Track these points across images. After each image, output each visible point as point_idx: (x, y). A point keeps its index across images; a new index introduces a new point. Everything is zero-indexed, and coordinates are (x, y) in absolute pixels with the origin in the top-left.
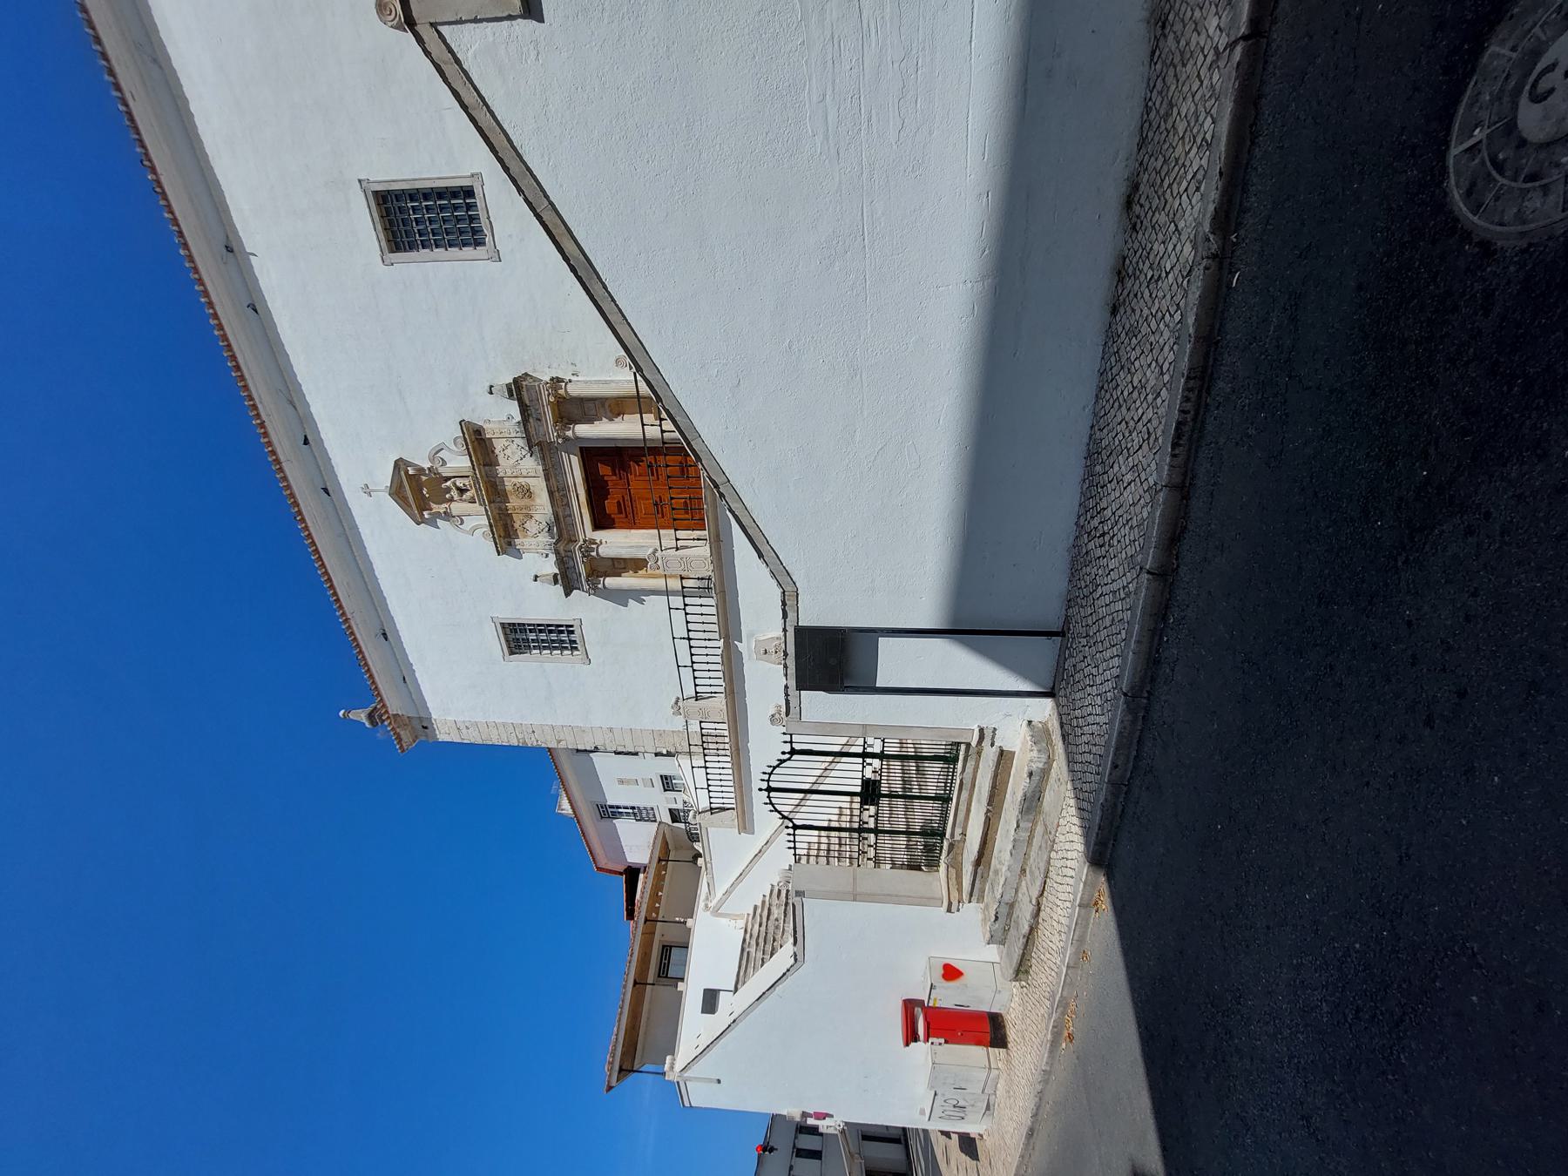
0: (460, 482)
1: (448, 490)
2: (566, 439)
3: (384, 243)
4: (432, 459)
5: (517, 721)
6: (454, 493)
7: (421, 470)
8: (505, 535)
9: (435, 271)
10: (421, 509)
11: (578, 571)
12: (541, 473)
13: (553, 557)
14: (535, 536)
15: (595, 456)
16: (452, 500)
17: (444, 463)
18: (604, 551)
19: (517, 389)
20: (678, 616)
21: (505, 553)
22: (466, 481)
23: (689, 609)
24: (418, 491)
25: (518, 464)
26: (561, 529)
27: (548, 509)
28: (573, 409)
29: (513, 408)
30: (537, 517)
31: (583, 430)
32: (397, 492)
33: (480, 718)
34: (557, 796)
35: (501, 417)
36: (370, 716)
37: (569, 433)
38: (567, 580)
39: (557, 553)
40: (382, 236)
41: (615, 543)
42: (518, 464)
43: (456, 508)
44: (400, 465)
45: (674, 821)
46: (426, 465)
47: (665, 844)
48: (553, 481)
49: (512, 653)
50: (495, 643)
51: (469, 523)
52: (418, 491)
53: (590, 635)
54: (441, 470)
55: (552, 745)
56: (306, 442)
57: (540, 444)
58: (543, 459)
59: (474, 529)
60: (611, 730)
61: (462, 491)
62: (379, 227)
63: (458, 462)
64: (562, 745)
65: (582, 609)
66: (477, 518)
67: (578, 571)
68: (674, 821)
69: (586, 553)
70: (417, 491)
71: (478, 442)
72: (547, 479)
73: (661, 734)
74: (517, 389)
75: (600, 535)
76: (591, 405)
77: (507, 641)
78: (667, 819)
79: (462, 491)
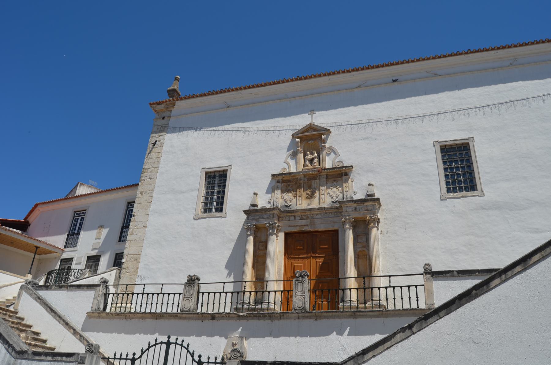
0: (316, 160)
1: (312, 154)
2: (344, 223)
3: (444, 144)
4: (330, 148)
5: (160, 170)
6: (310, 157)
7: (324, 142)
8: (284, 182)
9: (433, 168)
10: (301, 138)
11: (258, 223)
12: (322, 206)
13: (268, 206)
14: (283, 198)
15: (333, 239)
16: (305, 155)
17: (328, 154)
18: (272, 239)
19: (371, 201)
20: (219, 288)
21: (272, 179)
22: (317, 164)
23: (223, 295)
24: (311, 140)
25: (326, 197)
26: (286, 213)
27: (299, 207)
28: (363, 228)
29: (360, 196)
30: (294, 200)
31: (350, 235)
32: (311, 127)
33: (165, 148)
34: (91, 186)
35: (356, 189)
36: (174, 90)
37: (348, 226)
38: (252, 212)
39: (269, 210)
40: (447, 143)
41: (276, 245)
42: (326, 197)
43: (301, 156)
44: (327, 131)
45: (62, 260)
46: (327, 145)
47: (45, 252)
48: (318, 212)
49: (206, 173)
50: (215, 164)
51: (292, 163)
52: (311, 140)
53: (214, 222)
54: (324, 153)
55: (140, 189)
56: (394, 81)
57: (341, 207)
58: (331, 208)
59: (288, 164)
60: (145, 227)
61: (311, 161)
62: (452, 143)
63: (328, 162)
64: (139, 195)
65: (233, 220)
66: (295, 166)
67: (258, 223)
68: (62, 260)
69: (272, 226)
70: (311, 138)
71: (340, 175)
72: (319, 209)
73: (137, 260)
74: (371, 201)
75: (282, 235)
76: (364, 240)
77: (215, 172)
78: (65, 256)
79: (311, 161)
